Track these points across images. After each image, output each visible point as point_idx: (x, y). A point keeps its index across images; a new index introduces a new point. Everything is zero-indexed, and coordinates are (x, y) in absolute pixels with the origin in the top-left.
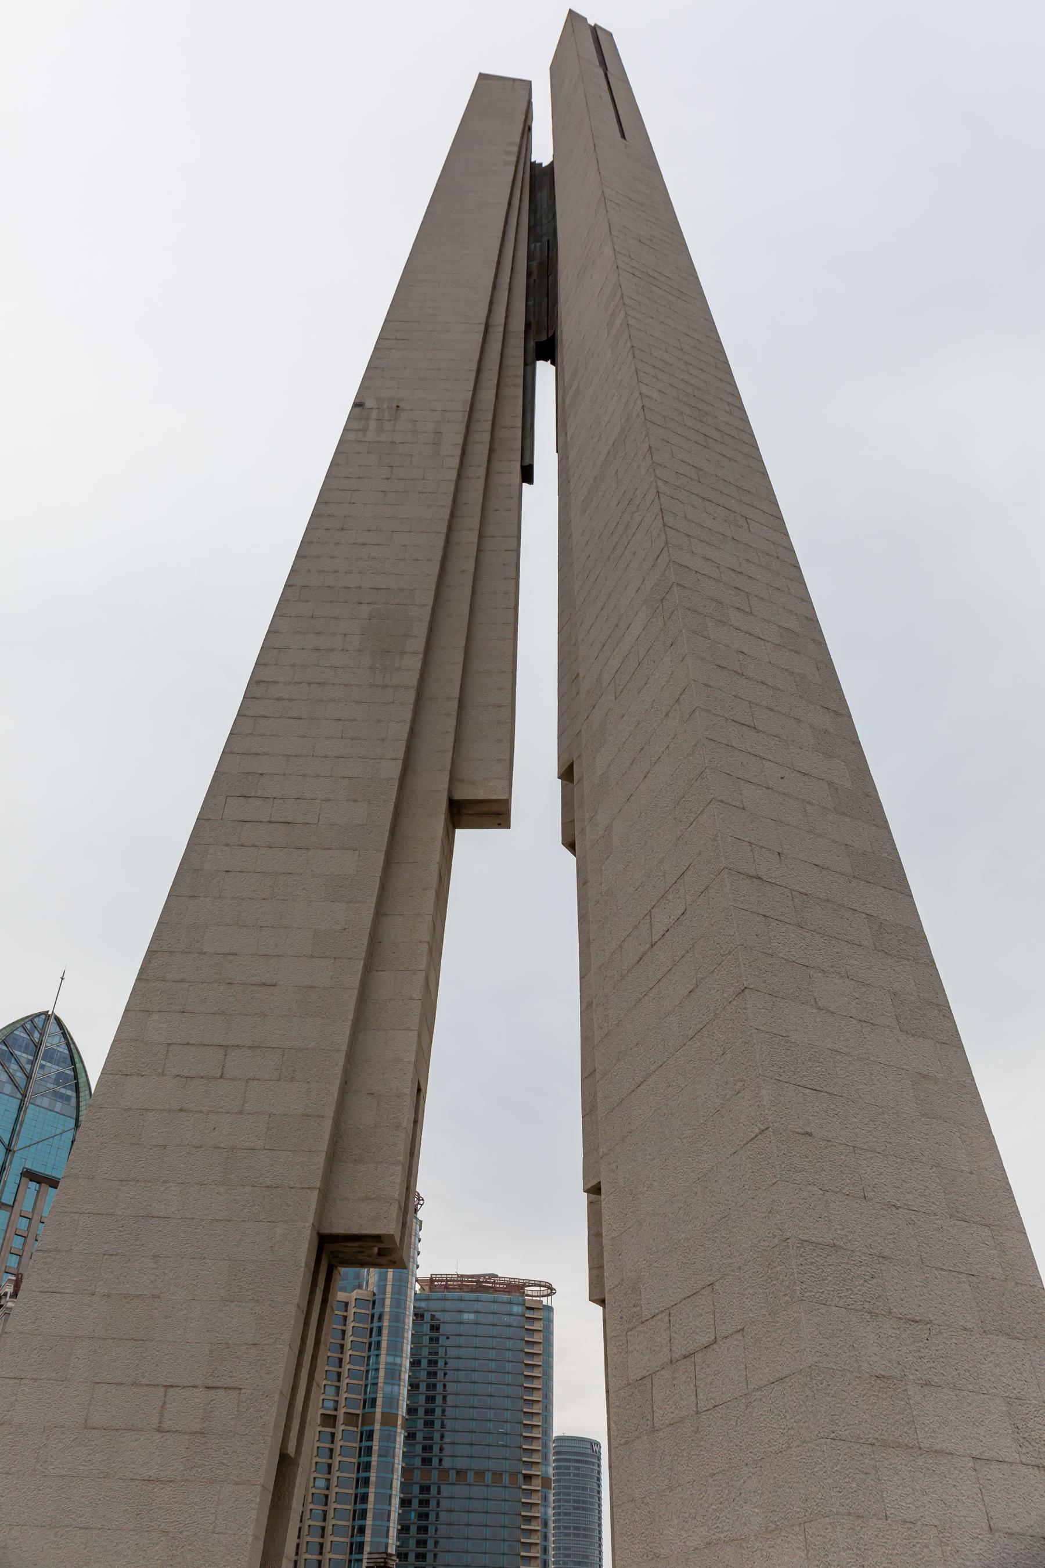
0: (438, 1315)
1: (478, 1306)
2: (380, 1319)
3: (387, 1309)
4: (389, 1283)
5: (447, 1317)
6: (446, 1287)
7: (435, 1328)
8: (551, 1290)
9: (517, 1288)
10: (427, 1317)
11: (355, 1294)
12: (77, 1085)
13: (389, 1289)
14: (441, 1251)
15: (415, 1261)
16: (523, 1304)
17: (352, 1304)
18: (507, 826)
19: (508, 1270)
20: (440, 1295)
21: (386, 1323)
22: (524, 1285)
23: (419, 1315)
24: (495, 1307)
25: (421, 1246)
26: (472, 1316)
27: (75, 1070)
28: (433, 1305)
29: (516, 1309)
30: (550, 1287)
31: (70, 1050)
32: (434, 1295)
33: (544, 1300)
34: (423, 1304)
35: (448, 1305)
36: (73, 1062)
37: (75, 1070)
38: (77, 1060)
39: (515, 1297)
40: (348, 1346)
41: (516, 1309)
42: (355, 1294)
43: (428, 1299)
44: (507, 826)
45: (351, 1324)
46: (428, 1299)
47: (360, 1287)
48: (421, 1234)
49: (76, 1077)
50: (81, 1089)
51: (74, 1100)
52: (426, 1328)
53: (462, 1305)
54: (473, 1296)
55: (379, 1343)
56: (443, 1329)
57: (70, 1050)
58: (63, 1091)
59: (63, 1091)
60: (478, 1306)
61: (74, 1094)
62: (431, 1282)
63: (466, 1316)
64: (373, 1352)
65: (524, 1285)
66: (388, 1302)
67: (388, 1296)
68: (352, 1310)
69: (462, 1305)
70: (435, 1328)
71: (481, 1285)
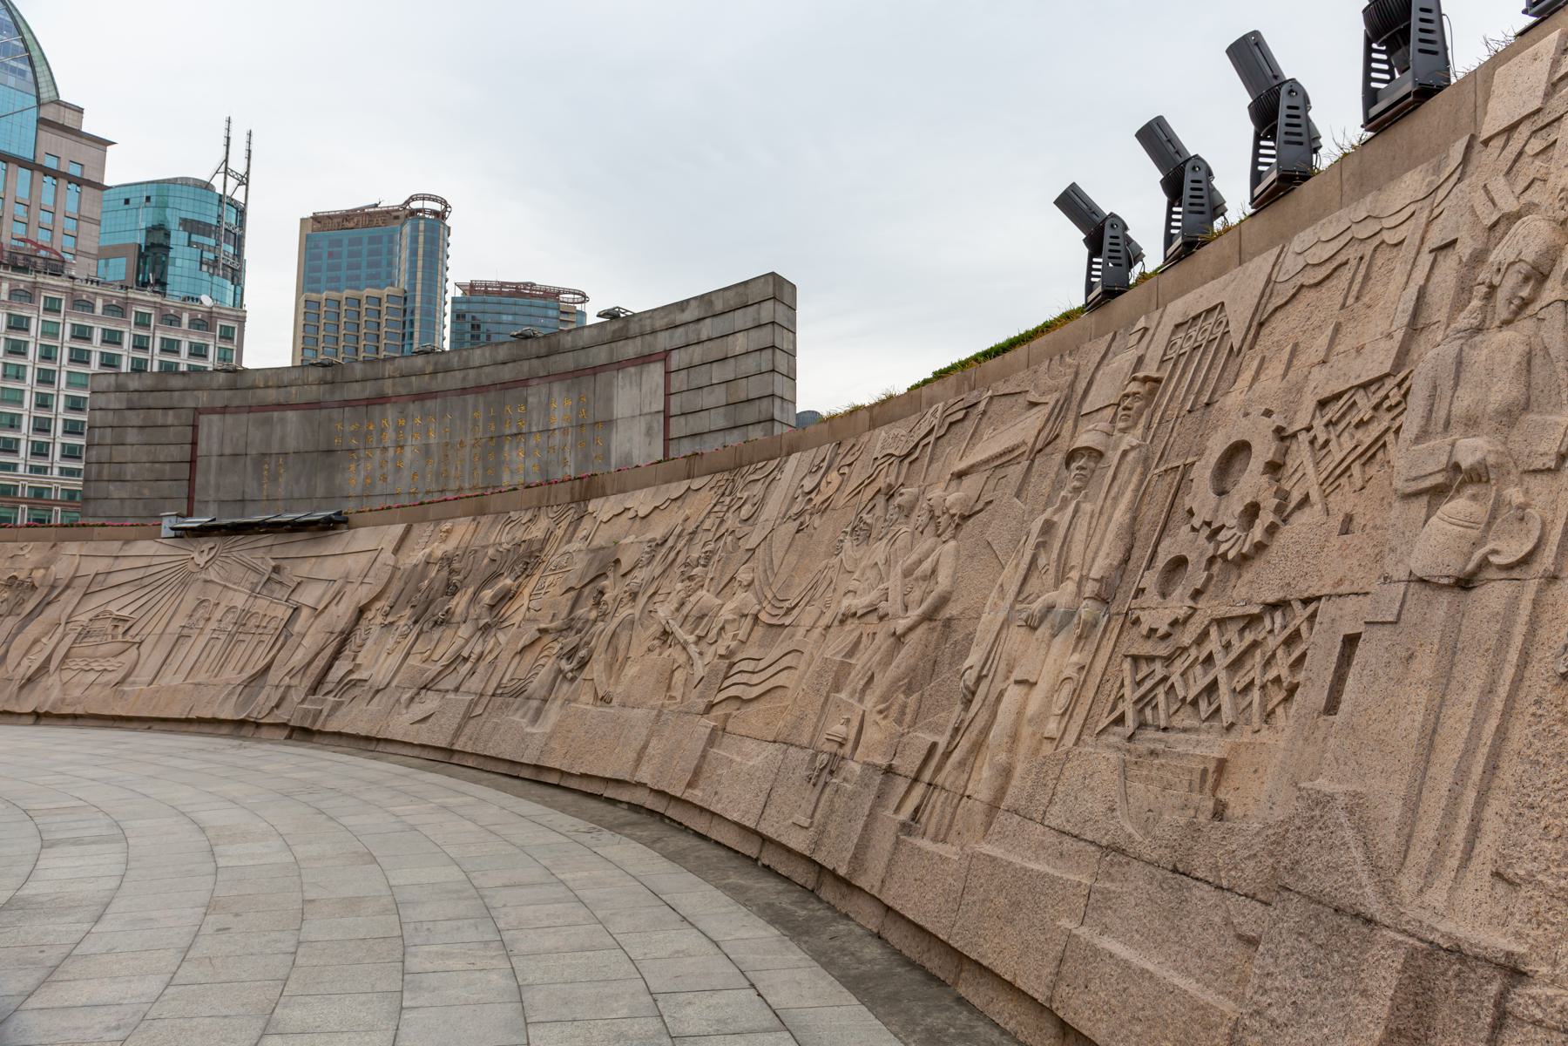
2: (413, 313)
3: (418, 305)
4: (419, 281)
5: (488, 318)
6: (486, 292)
7: (476, 327)
8: (584, 298)
9: (552, 295)
10: (469, 317)
11: (388, 290)
12: (30, 58)
13: (419, 287)
17: (364, 301)
18: (1074, 184)
20: (480, 298)
21: (417, 317)
22: (559, 293)
23: (458, 316)
24: (533, 311)
26: (510, 318)
27: (23, 41)
28: (472, 307)
29: (552, 313)
30: (584, 296)
31: (13, 17)
32: (474, 299)
33: (579, 307)
34: (464, 307)
35: (487, 307)
36: (20, 33)
37: (23, 41)
38: (24, 30)
40: (383, 336)
41: (552, 313)
42: (388, 290)
43: (469, 302)
44: (1074, 184)
45: (384, 317)
46: (469, 302)
47: (392, 285)
48: (450, 239)
49: (27, 49)
51: (30, 75)
52: (468, 327)
53: (500, 308)
55: (412, 334)
56: (483, 328)
57: (13, 17)
59: (13, 63)
62: (471, 288)
63: (504, 318)
64: (407, 341)
65: (559, 293)
66: (418, 299)
67: (418, 293)
68: (385, 305)
69: (500, 308)
70: (476, 327)
71: (519, 292)
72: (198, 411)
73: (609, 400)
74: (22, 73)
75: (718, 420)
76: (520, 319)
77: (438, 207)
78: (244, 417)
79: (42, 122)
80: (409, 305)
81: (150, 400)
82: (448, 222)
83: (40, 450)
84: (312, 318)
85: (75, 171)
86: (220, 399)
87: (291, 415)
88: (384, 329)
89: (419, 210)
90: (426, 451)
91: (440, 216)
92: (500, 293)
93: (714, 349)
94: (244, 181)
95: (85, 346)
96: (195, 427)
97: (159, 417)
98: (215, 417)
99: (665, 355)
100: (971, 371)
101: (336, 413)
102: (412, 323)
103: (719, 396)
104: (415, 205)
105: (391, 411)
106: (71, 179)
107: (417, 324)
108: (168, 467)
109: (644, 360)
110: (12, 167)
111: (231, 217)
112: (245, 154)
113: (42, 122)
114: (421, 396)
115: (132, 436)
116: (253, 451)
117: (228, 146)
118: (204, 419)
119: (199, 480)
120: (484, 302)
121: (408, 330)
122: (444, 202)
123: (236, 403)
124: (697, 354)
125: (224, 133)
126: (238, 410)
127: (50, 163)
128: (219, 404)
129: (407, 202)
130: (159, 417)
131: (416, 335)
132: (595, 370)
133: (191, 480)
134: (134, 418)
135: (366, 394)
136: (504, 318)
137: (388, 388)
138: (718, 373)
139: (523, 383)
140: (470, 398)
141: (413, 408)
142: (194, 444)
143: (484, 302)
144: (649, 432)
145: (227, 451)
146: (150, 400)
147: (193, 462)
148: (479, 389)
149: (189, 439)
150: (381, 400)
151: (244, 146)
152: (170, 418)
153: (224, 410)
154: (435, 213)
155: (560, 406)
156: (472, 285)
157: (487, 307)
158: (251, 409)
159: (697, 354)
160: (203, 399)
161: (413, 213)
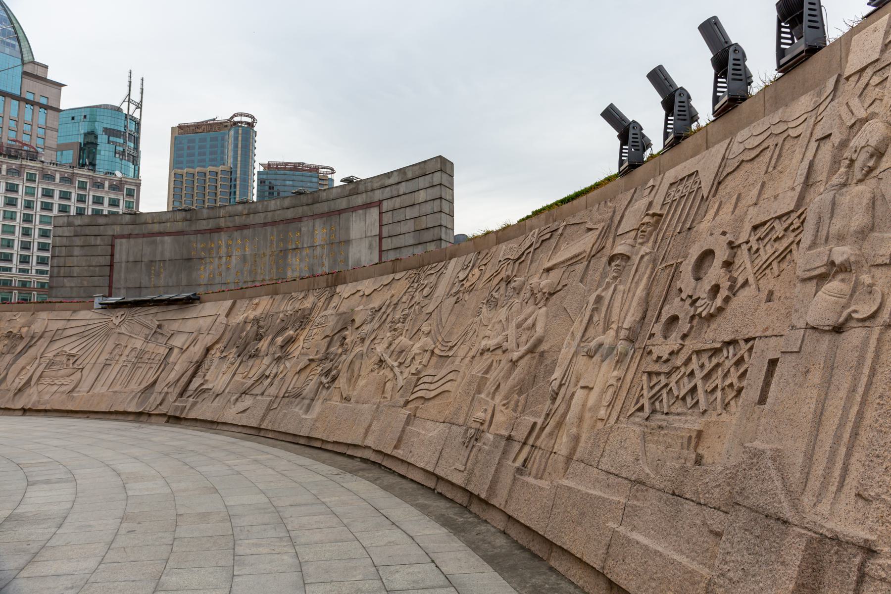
0: (273, 182)
1: (294, 178)
2: (235, 180)
3: (238, 176)
5: (278, 183)
7: (271, 188)
8: (333, 171)
9: (314, 169)
10: (267, 182)
11: (221, 168)
12: (18, 37)
13: (239, 165)
14: (690, 251)
15: (253, 152)
16: (318, 177)
18: (612, 104)
19: (311, 160)
21: (238, 182)
22: (318, 168)
23: (261, 182)
25: (256, 145)
26: (291, 183)
27: (14, 28)
28: (270, 177)
29: (315, 180)
30: (332, 170)
32: (270, 172)
33: (330, 176)
34: (265, 177)
35: (278, 177)
36: (12, 23)
37: (14, 28)
38: (14, 21)
39: (313, 174)
40: (219, 193)
42: (221, 168)
43: (267, 174)
44: (612, 104)
46: (267, 174)
49: (16, 33)
50: (21, 41)
51: (17, 47)
52: (267, 188)
54: (292, 172)
55: (235, 192)
56: (275, 189)
58: (8, 41)
59: (8, 41)
60: (294, 178)
61: (17, 44)
62: (269, 166)
63: (288, 183)
65: (318, 168)
66: (239, 172)
67: (239, 169)
68: (220, 176)
70: (271, 188)
71: (296, 168)
72: (114, 237)
73: (348, 229)
74: (13, 46)
75: (409, 240)
76: (296, 184)
77: (249, 120)
78: (140, 240)
79: (25, 74)
80: (233, 176)
81: (88, 230)
82: (255, 129)
83: (24, 260)
84: (178, 184)
85: (43, 101)
86: (127, 230)
87: (167, 239)
88: (219, 190)
89: (239, 122)
90: (244, 258)
91: (251, 125)
92: (285, 169)
93: (407, 200)
94: (139, 106)
95: (49, 201)
96: (113, 246)
97: (92, 240)
98: (124, 240)
99: (379, 203)
100: (554, 211)
101: (192, 238)
102: (235, 186)
103: (409, 226)
104: (236, 119)
105: (224, 236)
106: (41, 106)
107: (238, 187)
108: (97, 269)
109: (367, 206)
110: (8, 99)
111: (132, 127)
112: (140, 91)
113: (25, 74)
114: (241, 228)
115: (77, 251)
116: (145, 259)
117: (130, 86)
118: (117, 241)
119: (115, 276)
120: (276, 174)
121: (233, 190)
122: (252, 117)
123: (136, 232)
124: (397, 202)
125: (128, 79)
126: (137, 236)
127: (30, 97)
128: (126, 232)
129: (232, 118)
130: (92, 240)
131: (238, 193)
132: (340, 212)
133: (111, 276)
134: (78, 241)
135: (210, 227)
136: (288, 183)
137: (222, 223)
138: (410, 213)
139: (299, 219)
140: (269, 228)
141: (236, 234)
142: (112, 255)
143: (276, 174)
144: (370, 247)
145: (131, 259)
146: (88, 230)
147: (111, 266)
148: (274, 223)
149: (109, 253)
150: (218, 230)
151: (139, 86)
152: (99, 241)
153: (129, 236)
154: (248, 123)
155: (321, 232)
156: (269, 164)
157: (278, 177)
158: (144, 236)
159: (397, 202)
160: (117, 230)
161: (235, 123)
